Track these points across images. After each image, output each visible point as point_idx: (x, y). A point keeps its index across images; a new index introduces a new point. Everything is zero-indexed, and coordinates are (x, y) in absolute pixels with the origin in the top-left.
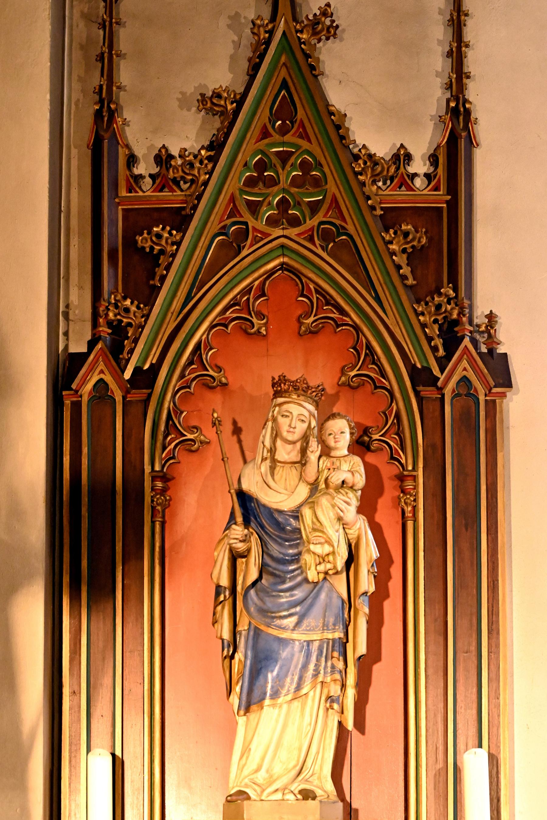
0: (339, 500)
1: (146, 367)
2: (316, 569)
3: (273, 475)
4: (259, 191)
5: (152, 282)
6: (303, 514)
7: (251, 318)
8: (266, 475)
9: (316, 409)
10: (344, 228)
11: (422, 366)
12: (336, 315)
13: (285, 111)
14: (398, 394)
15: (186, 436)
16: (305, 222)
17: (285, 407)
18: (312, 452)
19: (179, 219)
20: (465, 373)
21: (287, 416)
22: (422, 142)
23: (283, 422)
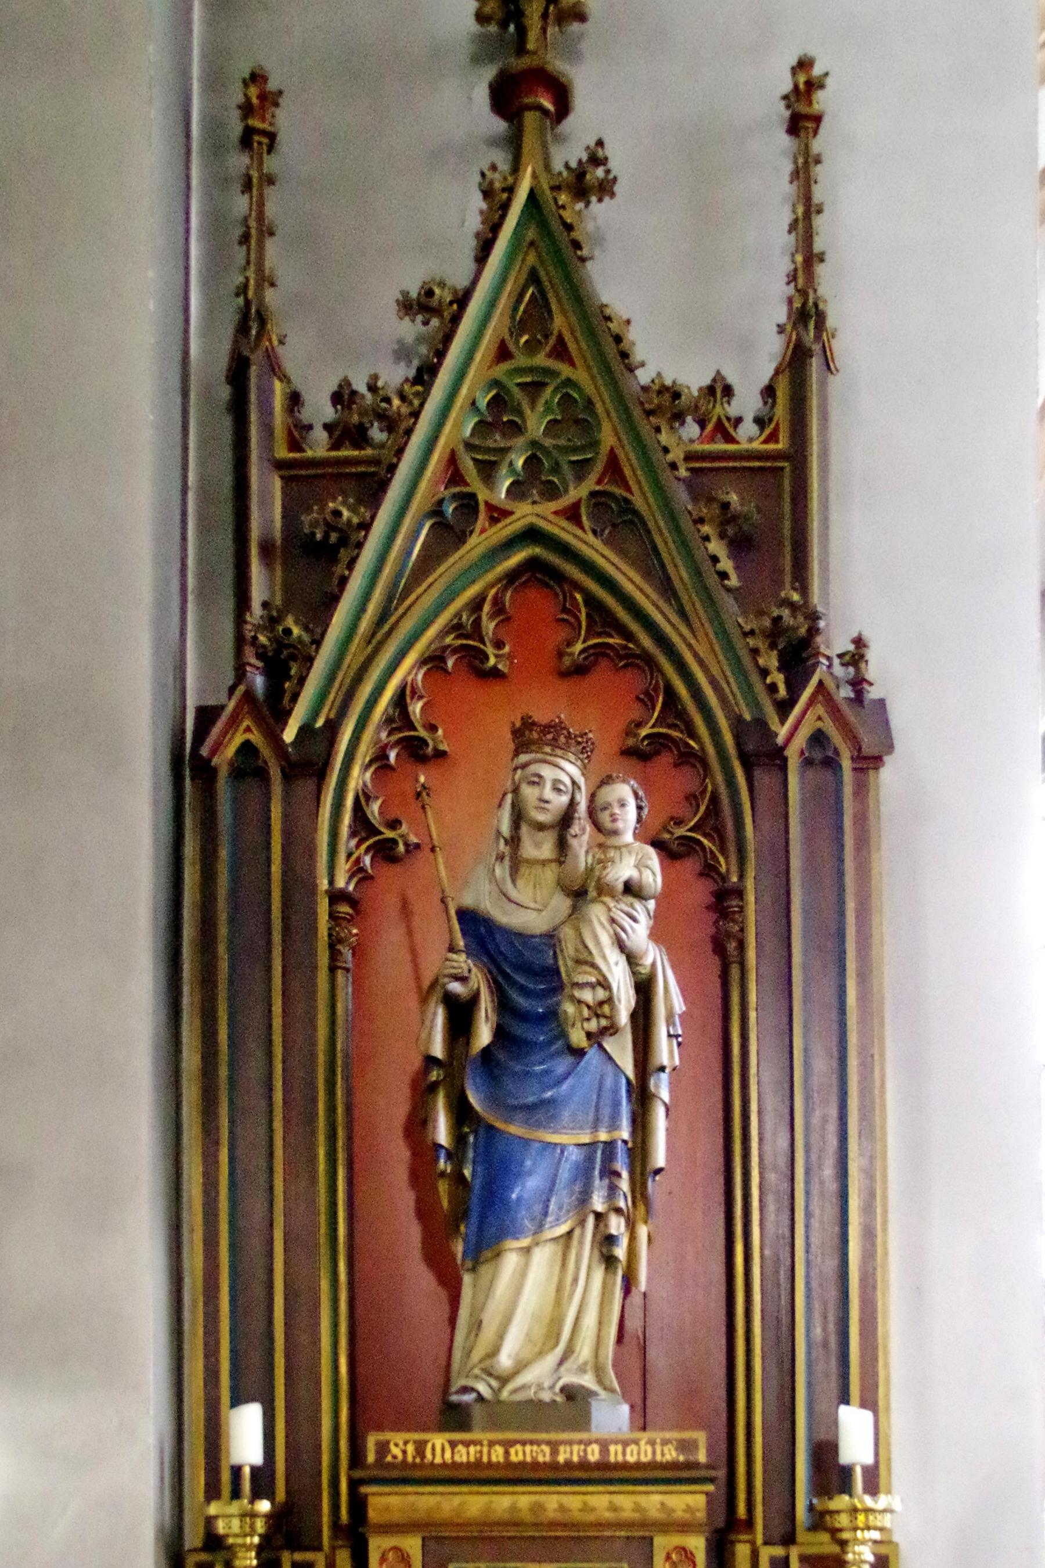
1: (320, 723)
3: (514, 881)
9: (583, 774)
10: (627, 501)
12: (615, 641)
13: (532, 319)
16: (566, 491)
18: (576, 836)
19: (372, 487)
22: (753, 369)
23: (529, 793)
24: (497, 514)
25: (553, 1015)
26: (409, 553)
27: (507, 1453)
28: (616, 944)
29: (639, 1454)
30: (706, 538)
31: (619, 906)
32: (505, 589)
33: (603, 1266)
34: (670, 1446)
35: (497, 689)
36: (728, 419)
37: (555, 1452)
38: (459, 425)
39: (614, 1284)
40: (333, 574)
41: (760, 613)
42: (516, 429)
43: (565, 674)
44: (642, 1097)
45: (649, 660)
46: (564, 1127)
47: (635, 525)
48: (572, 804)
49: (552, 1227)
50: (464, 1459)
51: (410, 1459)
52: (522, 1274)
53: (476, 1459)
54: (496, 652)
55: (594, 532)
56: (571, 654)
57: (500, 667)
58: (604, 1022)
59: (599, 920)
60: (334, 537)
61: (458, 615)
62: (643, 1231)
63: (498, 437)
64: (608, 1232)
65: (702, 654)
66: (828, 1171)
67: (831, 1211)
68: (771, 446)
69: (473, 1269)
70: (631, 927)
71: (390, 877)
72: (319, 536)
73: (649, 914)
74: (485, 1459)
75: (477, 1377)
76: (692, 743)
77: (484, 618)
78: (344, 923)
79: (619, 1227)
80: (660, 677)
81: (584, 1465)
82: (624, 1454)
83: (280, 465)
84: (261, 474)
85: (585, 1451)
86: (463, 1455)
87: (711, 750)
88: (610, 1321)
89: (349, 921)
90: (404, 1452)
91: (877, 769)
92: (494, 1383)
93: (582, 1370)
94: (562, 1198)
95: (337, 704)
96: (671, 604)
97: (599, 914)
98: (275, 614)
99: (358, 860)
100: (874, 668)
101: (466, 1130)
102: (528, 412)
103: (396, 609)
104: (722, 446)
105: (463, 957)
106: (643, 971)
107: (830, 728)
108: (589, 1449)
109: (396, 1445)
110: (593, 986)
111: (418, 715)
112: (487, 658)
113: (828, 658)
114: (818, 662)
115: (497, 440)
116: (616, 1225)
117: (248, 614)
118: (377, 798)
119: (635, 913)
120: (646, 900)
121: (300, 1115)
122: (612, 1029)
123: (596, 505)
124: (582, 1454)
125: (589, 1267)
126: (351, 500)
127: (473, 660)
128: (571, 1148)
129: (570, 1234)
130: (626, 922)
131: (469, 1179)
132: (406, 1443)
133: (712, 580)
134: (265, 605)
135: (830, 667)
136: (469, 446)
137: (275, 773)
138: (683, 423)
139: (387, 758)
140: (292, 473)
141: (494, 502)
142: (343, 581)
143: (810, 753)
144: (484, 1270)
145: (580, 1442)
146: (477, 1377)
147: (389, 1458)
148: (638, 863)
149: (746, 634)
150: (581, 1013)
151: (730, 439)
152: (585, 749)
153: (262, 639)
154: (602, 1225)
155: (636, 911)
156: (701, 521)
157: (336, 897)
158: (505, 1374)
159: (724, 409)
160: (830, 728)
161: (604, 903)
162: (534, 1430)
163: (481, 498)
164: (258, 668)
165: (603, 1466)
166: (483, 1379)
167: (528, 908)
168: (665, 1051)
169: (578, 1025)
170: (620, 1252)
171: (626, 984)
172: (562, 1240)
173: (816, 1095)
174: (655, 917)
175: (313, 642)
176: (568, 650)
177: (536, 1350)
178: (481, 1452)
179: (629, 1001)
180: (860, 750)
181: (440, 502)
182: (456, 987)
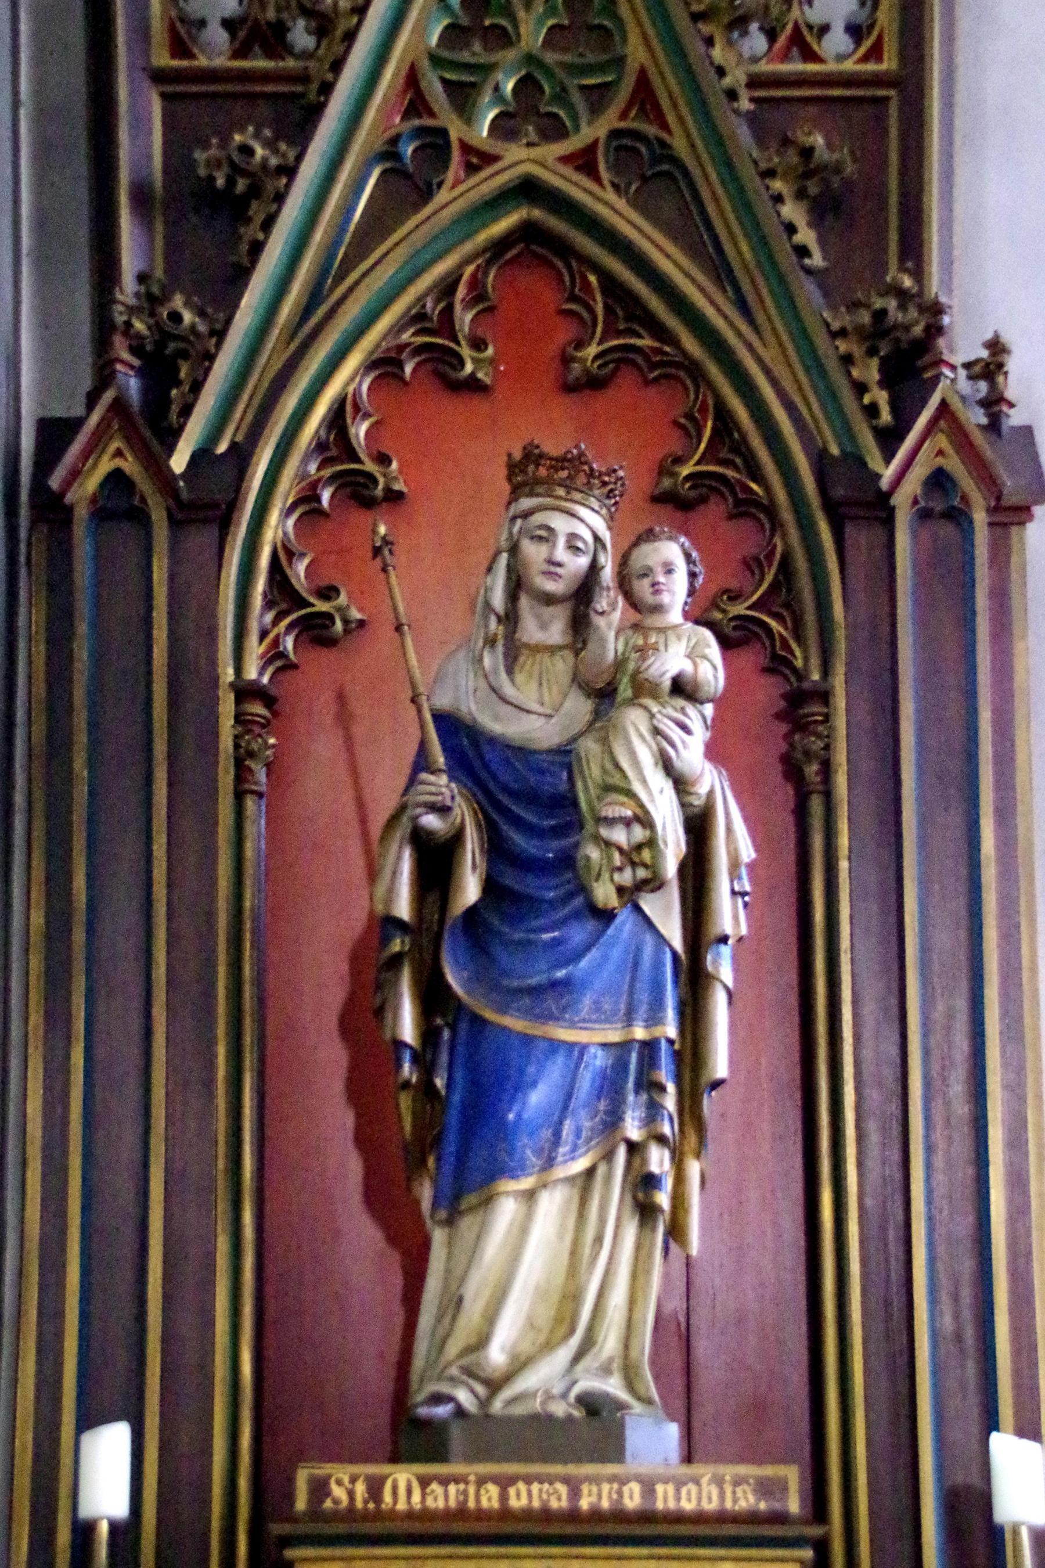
0: (666, 720)
1: (222, 448)
2: (612, 880)
3: (510, 671)
4: (473, 60)
5: (233, 258)
6: (583, 755)
7: (456, 347)
8: (495, 671)
10: (663, 144)
11: (842, 451)
12: (646, 342)
14: (787, 516)
15: (313, 605)
16: (577, 128)
17: (538, 518)
19: (298, 117)
20: (940, 461)
21: (540, 538)
23: (533, 552)
24: (478, 159)
25: (568, 861)
26: (348, 219)
27: (504, 1497)
28: (660, 766)
29: (699, 1499)
30: (778, 199)
31: (664, 711)
32: (489, 263)
33: (637, 1217)
34: (745, 1487)
35: (479, 405)
36: (810, 27)
37: (575, 1493)
38: (421, 29)
39: (652, 1244)
40: (240, 238)
41: (855, 305)
42: (503, 38)
43: (569, 388)
44: (694, 980)
45: (695, 371)
46: (584, 1020)
47: (674, 179)
48: (594, 568)
49: (566, 1161)
50: (441, 1504)
51: (359, 1504)
52: (523, 1230)
53: (458, 1502)
54: (475, 354)
55: (615, 186)
56: (582, 361)
57: (480, 375)
58: (642, 873)
59: (638, 730)
60: (241, 185)
61: (420, 299)
62: (694, 1168)
63: (477, 47)
64: (645, 1170)
65: (768, 361)
66: (958, 1087)
67: (963, 1147)
68: (871, 67)
69: (450, 1222)
70: (683, 742)
71: (320, 670)
72: (220, 182)
73: (705, 722)
74: (471, 1504)
75: (452, 1379)
76: (754, 486)
77: (458, 307)
78: (257, 730)
79: (661, 1163)
80: (709, 393)
81: (619, 1515)
82: (678, 1499)
83: (159, 77)
84: (132, 81)
85: (620, 1493)
86: (440, 1498)
87: (781, 496)
88: (646, 1298)
89: (263, 726)
90: (351, 1494)
91: (1022, 524)
92: (480, 1389)
93: (606, 1370)
94: (581, 1120)
95: (249, 417)
96: (725, 291)
97: (637, 722)
98: (155, 290)
99: (276, 642)
100: (1018, 380)
101: (439, 1021)
102: (521, 14)
103: (332, 290)
104: (797, 67)
105: (444, 779)
106: (696, 803)
107: (954, 465)
108: (626, 1489)
109: (339, 1483)
110: (627, 823)
111: (363, 442)
112: (462, 364)
113: (953, 368)
114: (941, 374)
115: (476, 52)
116: (658, 1160)
117: (117, 289)
118: (303, 555)
119: (687, 722)
120: (702, 703)
121: (193, 998)
122: (654, 883)
123: (618, 149)
124: (615, 1496)
125: (618, 1220)
126: (267, 132)
127: (441, 363)
128: (592, 1050)
129: (590, 1173)
130: (675, 733)
131: (443, 1093)
132: (353, 1480)
133: (786, 259)
134: (142, 278)
135: (953, 381)
136: (435, 60)
137: (158, 516)
138: (745, 33)
139: (318, 499)
140: (179, 88)
141: (474, 143)
142: (257, 249)
143: (926, 502)
144: (467, 1224)
145: (612, 1479)
146: (452, 1379)
147: (328, 1504)
148: (689, 652)
149: (834, 335)
150: (610, 859)
151: (810, 55)
152: (609, 490)
153: (139, 325)
154: (637, 1161)
155: (690, 718)
156: (770, 173)
157: (245, 692)
158: (497, 1375)
159: (803, 13)
160: (954, 465)
161: (646, 709)
162: (544, 1460)
163: (454, 136)
164: (132, 367)
165: (647, 1517)
166: (462, 1382)
167: (533, 712)
168: (728, 915)
169: (606, 876)
170: (663, 1199)
171: (674, 820)
172: (579, 1182)
173: (936, 979)
174: (713, 727)
175: (212, 333)
176: (579, 354)
177: (542, 1338)
178: (465, 1493)
179: (678, 845)
180: (999, 498)
181: (394, 141)
182: (431, 821)
